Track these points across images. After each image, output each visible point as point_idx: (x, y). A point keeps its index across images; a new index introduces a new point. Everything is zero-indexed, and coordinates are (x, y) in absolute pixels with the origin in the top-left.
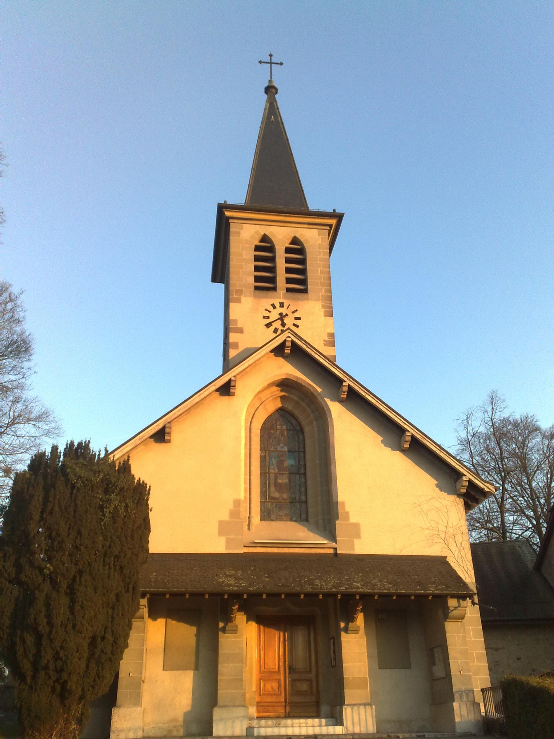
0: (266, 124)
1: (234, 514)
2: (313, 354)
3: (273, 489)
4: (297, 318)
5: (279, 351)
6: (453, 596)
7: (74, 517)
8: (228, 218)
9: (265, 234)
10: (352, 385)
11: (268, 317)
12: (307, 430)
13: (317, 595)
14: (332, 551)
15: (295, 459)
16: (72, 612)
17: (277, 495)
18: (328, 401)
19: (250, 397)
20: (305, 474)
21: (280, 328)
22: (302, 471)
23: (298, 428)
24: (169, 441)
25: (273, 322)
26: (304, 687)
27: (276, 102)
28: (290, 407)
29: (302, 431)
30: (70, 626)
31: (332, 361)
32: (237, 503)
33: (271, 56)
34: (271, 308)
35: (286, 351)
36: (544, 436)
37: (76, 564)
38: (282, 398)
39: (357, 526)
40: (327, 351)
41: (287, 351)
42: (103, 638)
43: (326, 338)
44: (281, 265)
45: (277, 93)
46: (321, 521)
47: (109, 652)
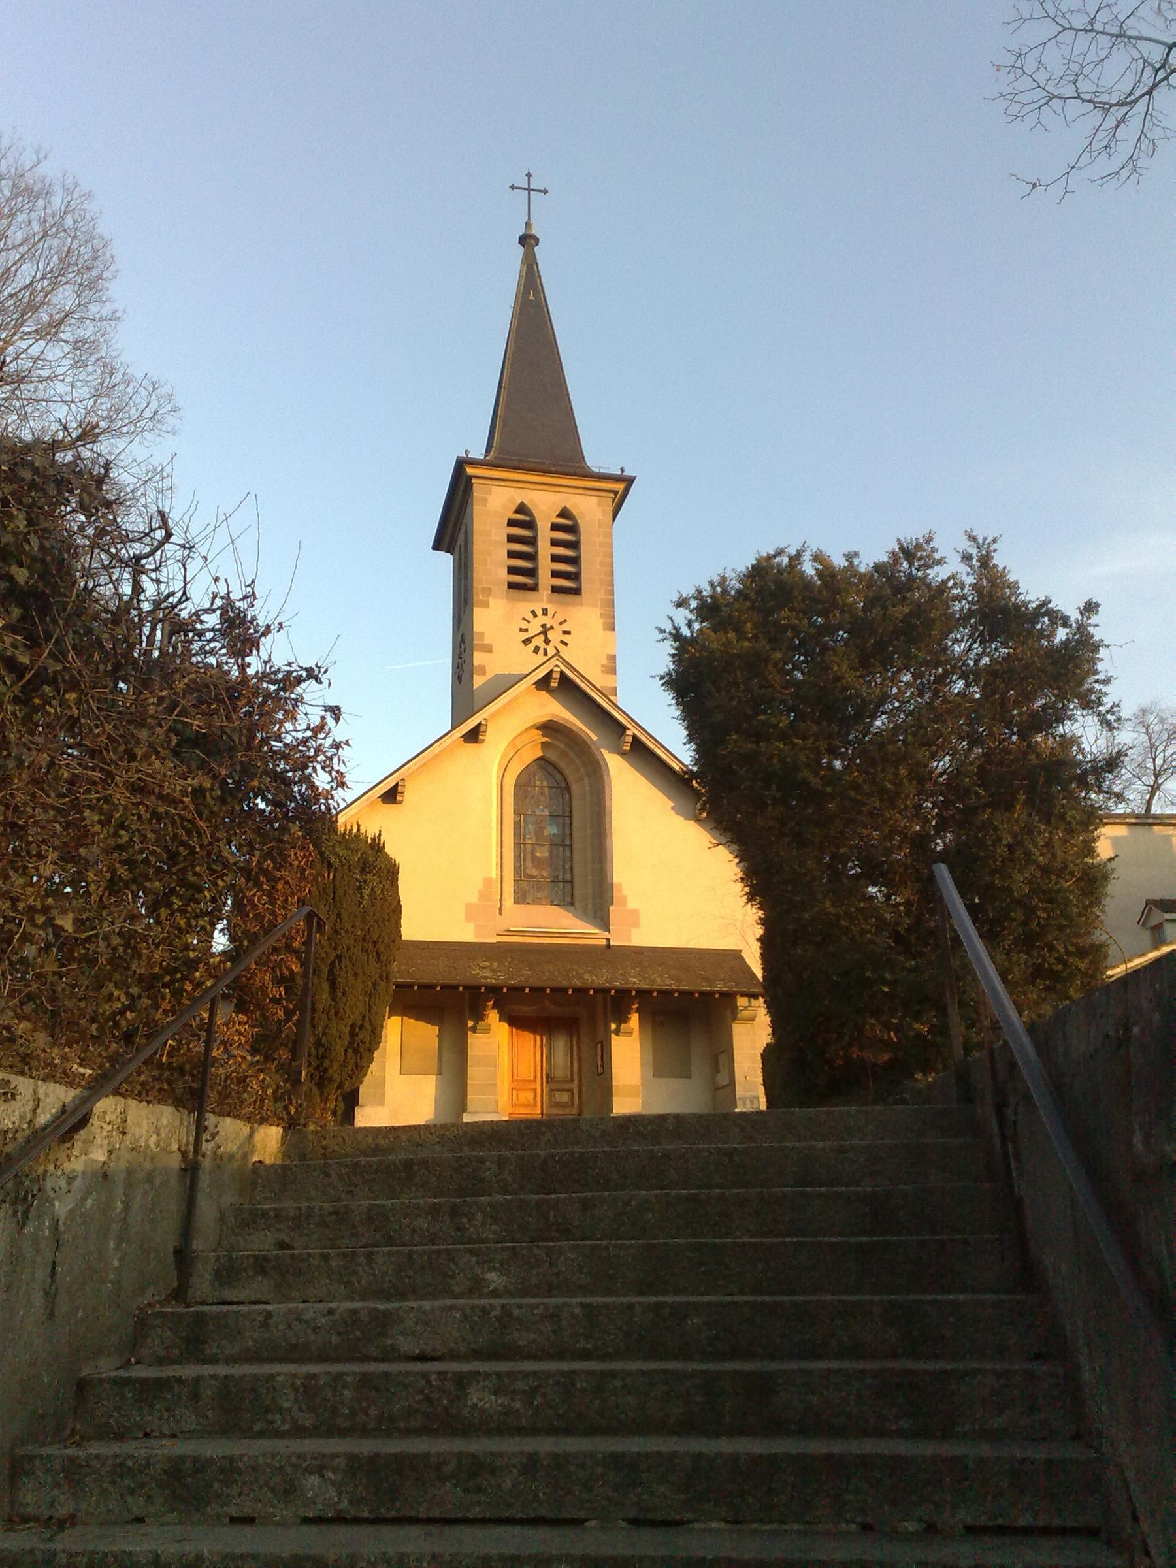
0: (521, 306)
1: (484, 896)
2: (588, 690)
3: (529, 864)
5: (543, 684)
6: (743, 995)
7: (333, 898)
8: (470, 478)
9: (522, 503)
10: (638, 734)
11: (526, 630)
12: (575, 788)
13: (586, 990)
14: (604, 942)
15: (558, 826)
16: (333, 998)
17: (534, 872)
18: (605, 752)
19: (503, 744)
20: (571, 846)
21: (543, 646)
22: (568, 842)
23: (563, 785)
24: (401, 802)
25: (533, 637)
26: (565, 1097)
27: (537, 264)
28: (553, 756)
29: (568, 789)
30: (332, 1012)
32: (488, 882)
33: (529, 175)
34: (530, 617)
35: (552, 685)
37: (335, 949)
39: (635, 914)
41: (554, 684)
42: (361, 1027)
44: (545, 550)
45: (537, 244)
46: (590, 906)
47: (368, 1042)
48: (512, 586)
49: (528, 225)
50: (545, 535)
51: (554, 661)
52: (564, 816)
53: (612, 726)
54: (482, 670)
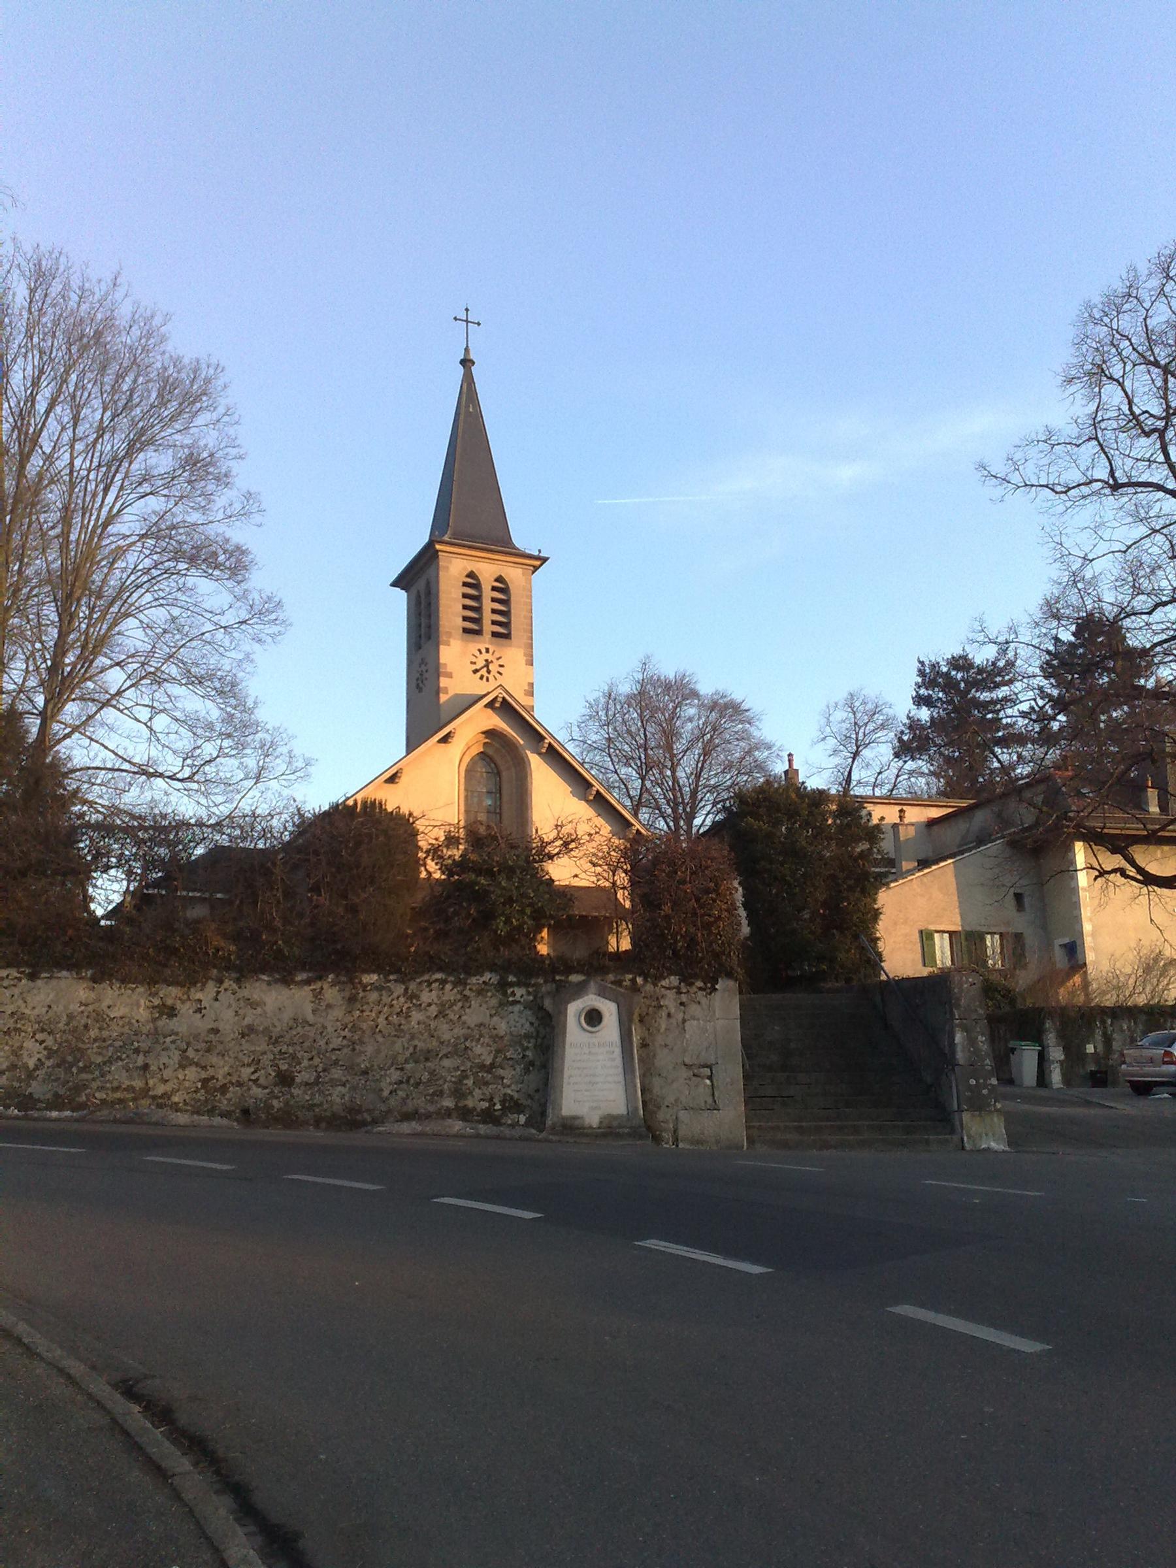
4: (501, 666)
5: (490, 705)
8: (438, 551)
11: (475, 663)
12: (504, 774)
21: (486, 675)
28: (490, 752)
31: (530, 709)
36: (702, 706)
38: (485, 744)
40: (524, 700)
41: (497, 705)
43: (527, 688)
44: (488, 605)
48: (466, 631)
49: (467, 350)
50: (487, 594)
51: (499, 690)
52: (497, 792)
53: (535, 735)
54: (446, 690)
